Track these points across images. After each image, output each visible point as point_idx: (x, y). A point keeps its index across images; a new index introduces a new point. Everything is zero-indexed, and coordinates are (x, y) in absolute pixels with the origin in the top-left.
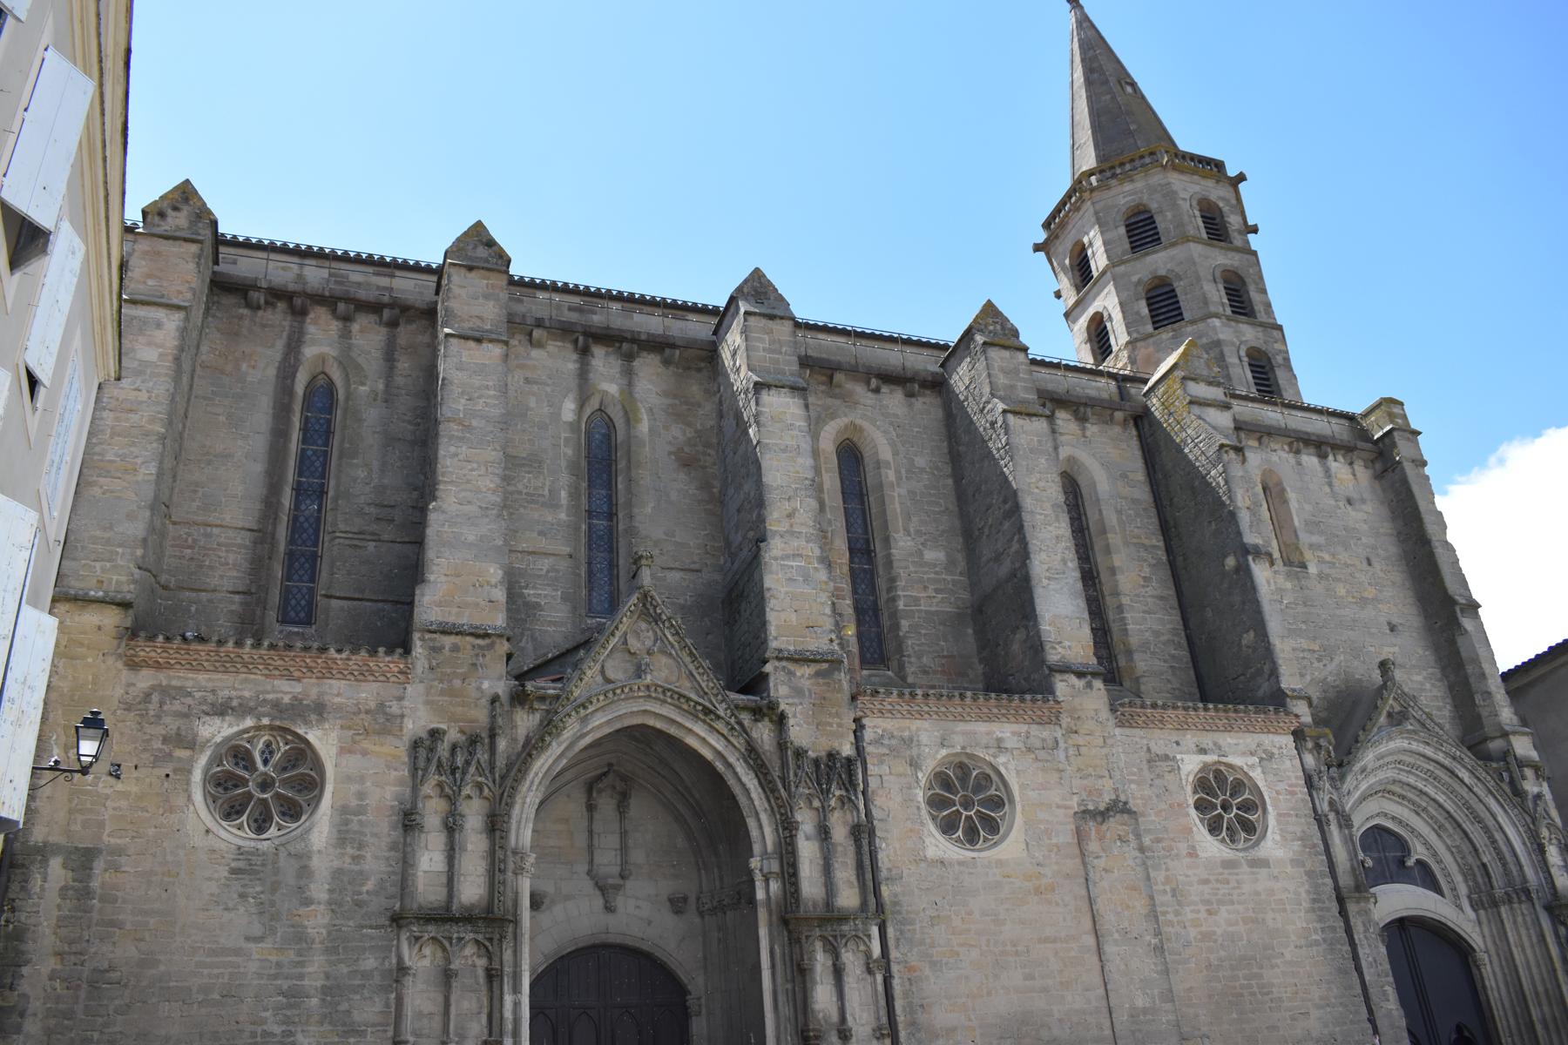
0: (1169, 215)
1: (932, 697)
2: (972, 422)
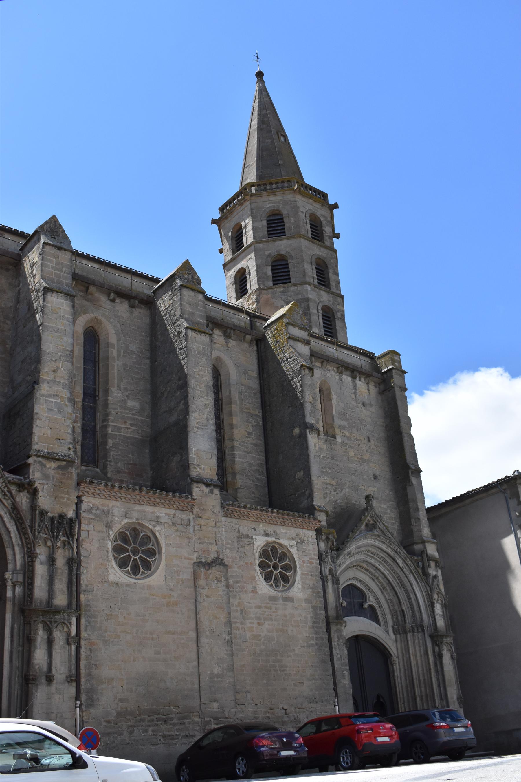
0: (292, 220)
1: (124, 489)
2: (166, 329)
